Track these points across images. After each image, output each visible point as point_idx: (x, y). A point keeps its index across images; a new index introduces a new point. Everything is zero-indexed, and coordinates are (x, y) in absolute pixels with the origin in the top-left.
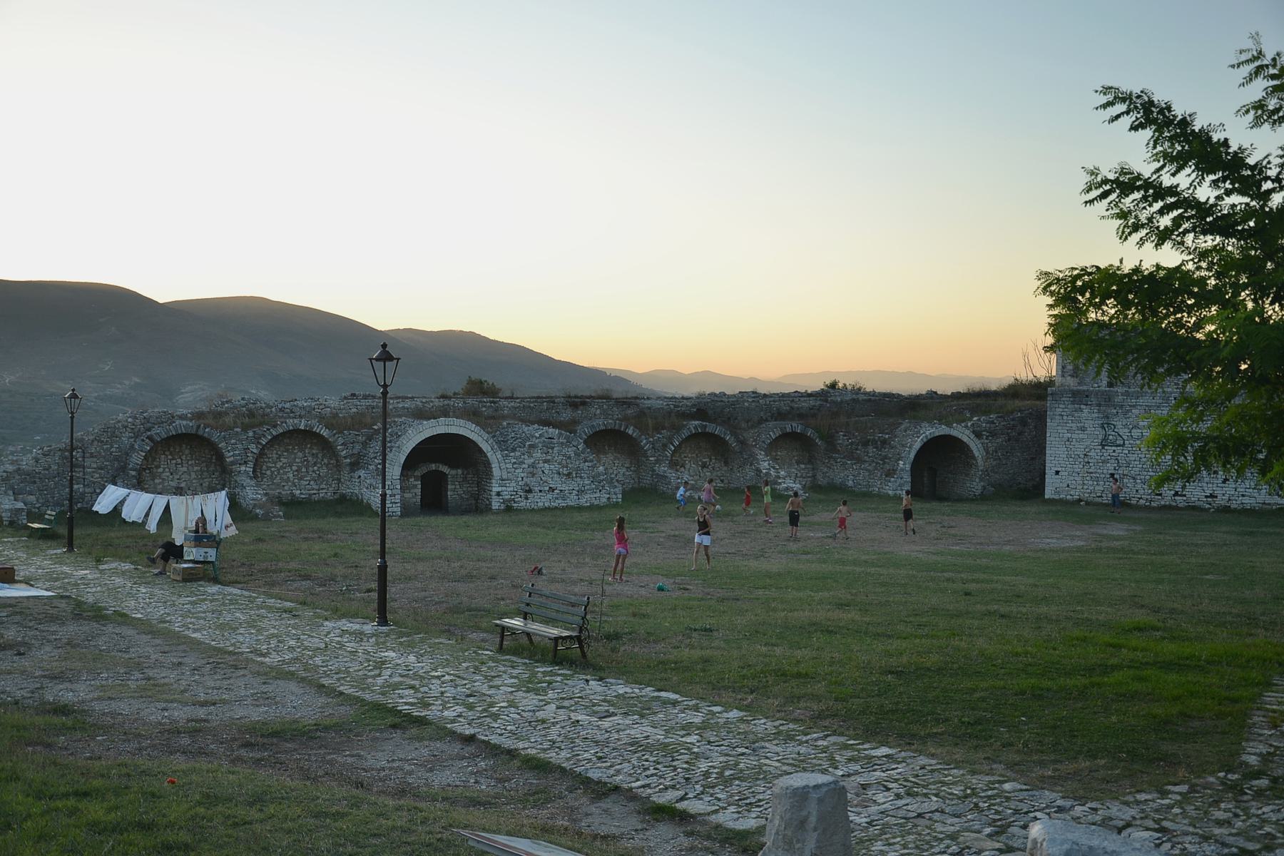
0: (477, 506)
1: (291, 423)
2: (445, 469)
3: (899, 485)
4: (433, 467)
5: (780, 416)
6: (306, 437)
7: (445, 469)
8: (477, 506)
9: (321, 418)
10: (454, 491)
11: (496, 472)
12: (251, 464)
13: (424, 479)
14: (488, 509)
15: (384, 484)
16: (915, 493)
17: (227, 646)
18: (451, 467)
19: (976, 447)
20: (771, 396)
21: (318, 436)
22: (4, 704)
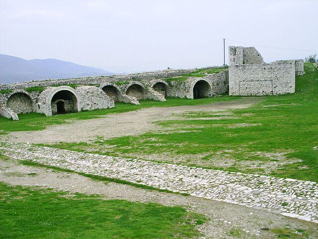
0: (73, 111)
1: (15, 92)
2: (63, 100)
3: (191, 95)
4: (60, 100)
5: (156, 78)
6: (20, 95)
7: (63, 100)
8: (73, 111)
9: (25, 89)
10: (67, 107)
11: (78, 100)
12: (6, 104)
13: (58, 104)
14: (77, 111)
15: (45, 104)
16: (195, 97)
17: (60, 162)
18: (65, 100)
19: (210, 84)
20: (39, 60)
21: (25, 94)
22: (2, 185)
